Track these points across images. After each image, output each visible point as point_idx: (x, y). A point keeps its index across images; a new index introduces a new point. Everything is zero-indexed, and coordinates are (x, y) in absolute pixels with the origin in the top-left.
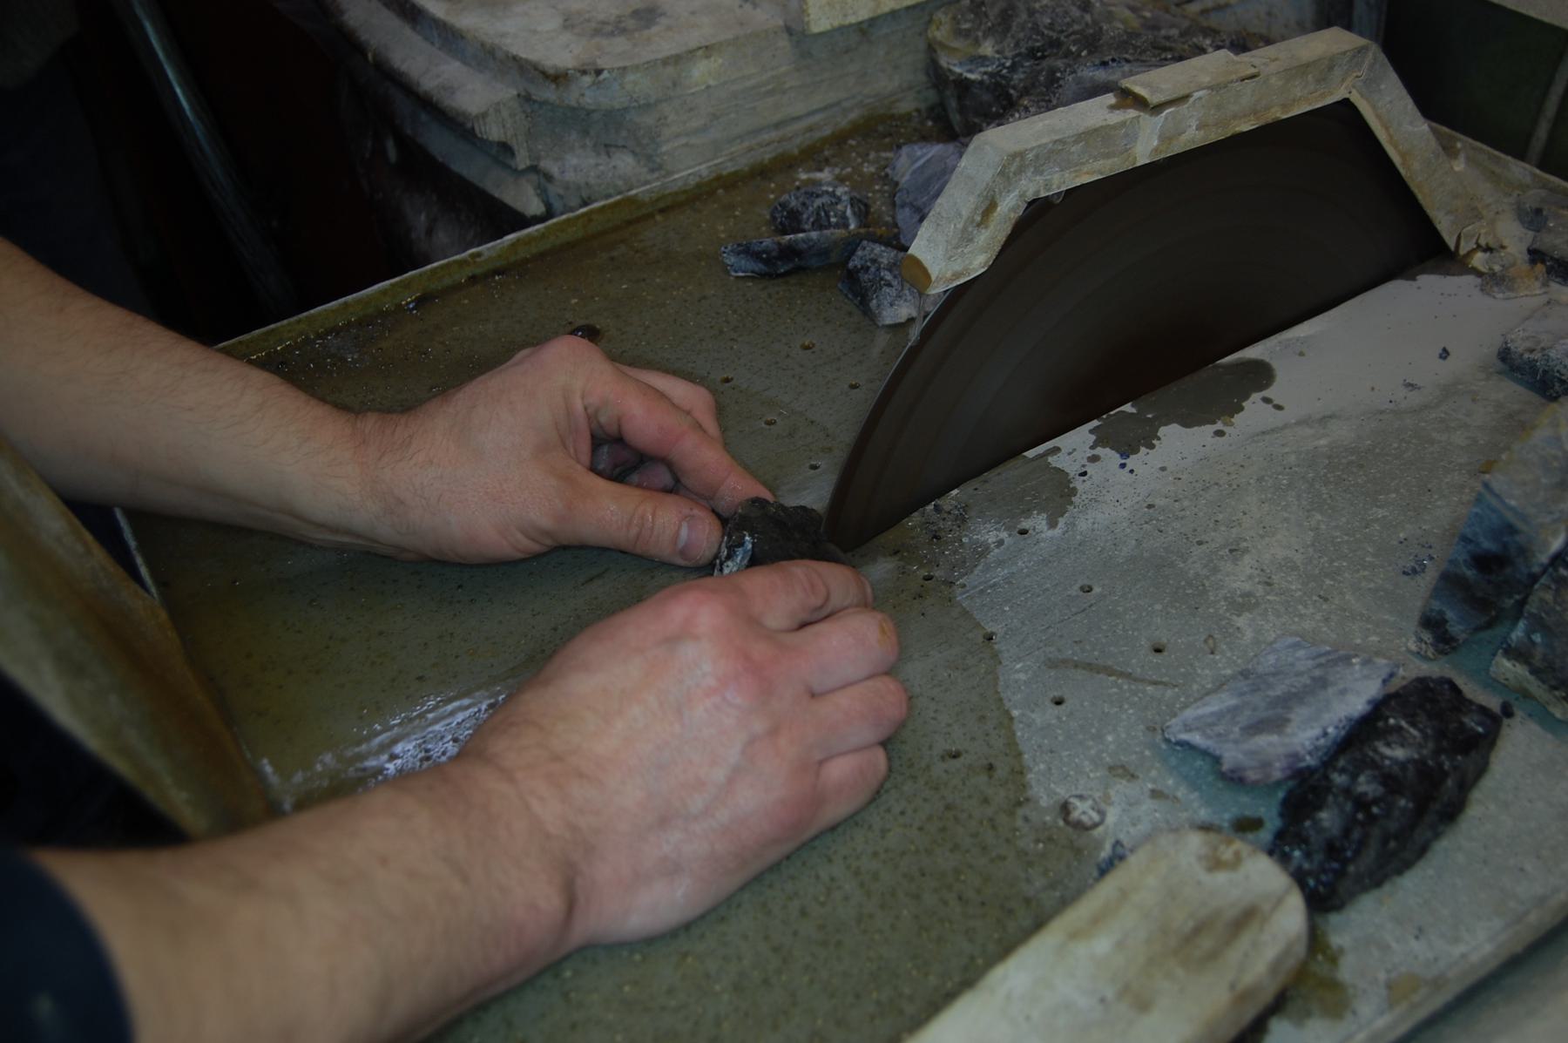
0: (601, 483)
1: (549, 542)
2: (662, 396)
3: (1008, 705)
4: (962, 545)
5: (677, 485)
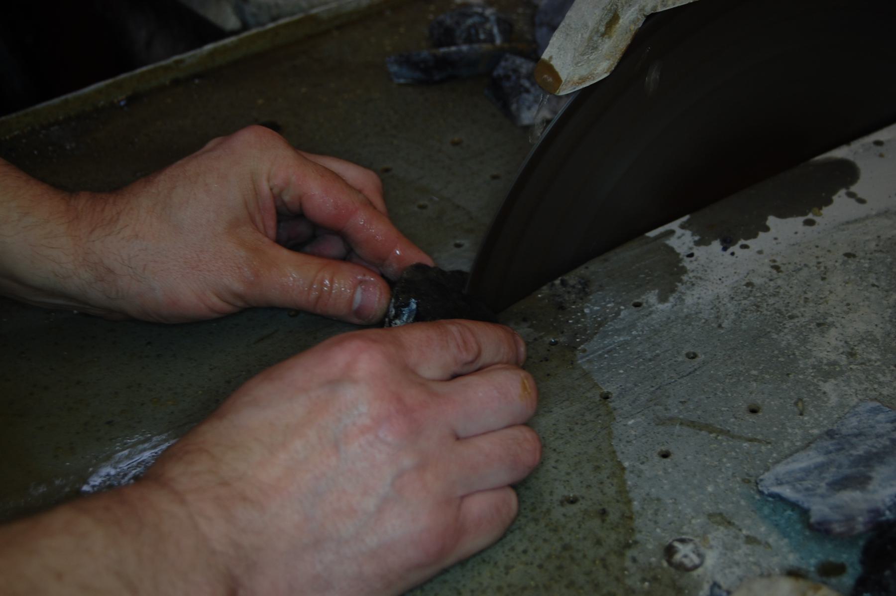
0: (285, 253)
1: (240, 304)
2: (337, 177)
3: (620, 457)
4: (584, 315)
5: (350, 252)
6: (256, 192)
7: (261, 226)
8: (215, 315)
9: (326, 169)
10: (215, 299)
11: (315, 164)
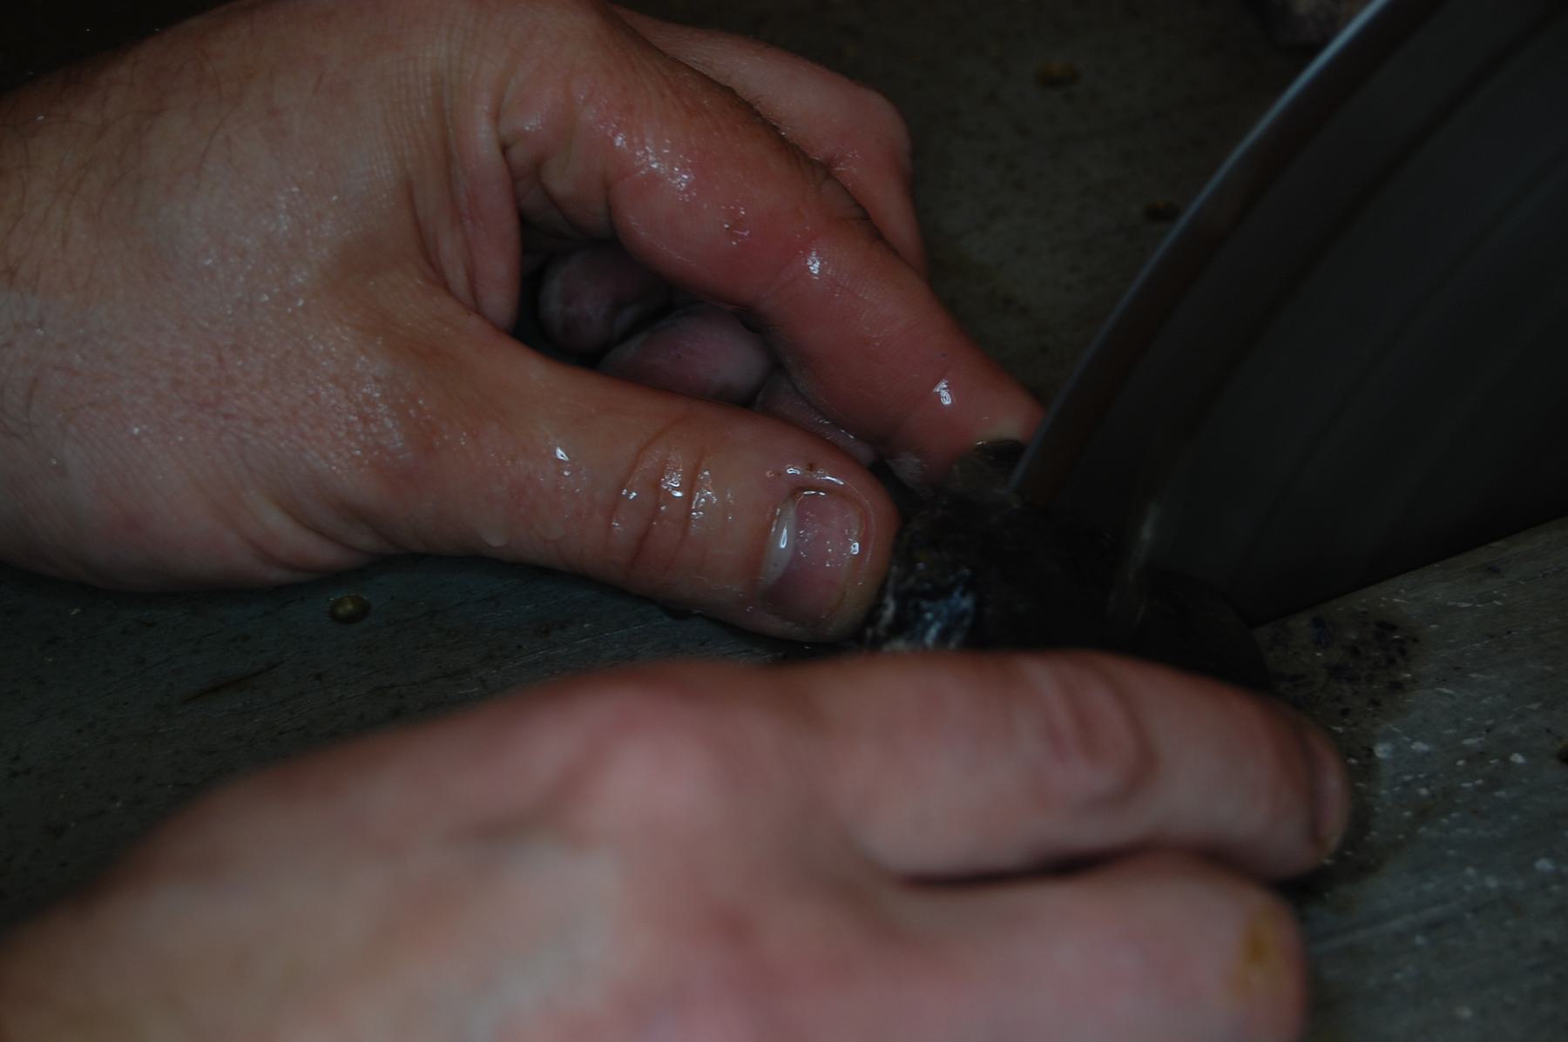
0: (532, 373)
1: (366, 541)
2: (747, 113)
5: (782, 385)
6: (448, 154)
7: (457, 277)
8: (277, 575)
9: (709, 83)
10: (276, 523)
11: (676, 63)
